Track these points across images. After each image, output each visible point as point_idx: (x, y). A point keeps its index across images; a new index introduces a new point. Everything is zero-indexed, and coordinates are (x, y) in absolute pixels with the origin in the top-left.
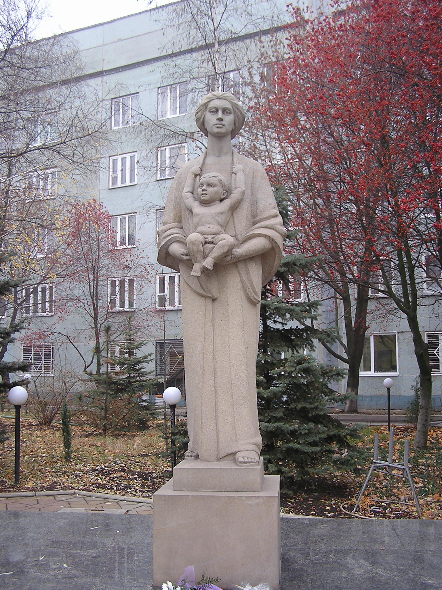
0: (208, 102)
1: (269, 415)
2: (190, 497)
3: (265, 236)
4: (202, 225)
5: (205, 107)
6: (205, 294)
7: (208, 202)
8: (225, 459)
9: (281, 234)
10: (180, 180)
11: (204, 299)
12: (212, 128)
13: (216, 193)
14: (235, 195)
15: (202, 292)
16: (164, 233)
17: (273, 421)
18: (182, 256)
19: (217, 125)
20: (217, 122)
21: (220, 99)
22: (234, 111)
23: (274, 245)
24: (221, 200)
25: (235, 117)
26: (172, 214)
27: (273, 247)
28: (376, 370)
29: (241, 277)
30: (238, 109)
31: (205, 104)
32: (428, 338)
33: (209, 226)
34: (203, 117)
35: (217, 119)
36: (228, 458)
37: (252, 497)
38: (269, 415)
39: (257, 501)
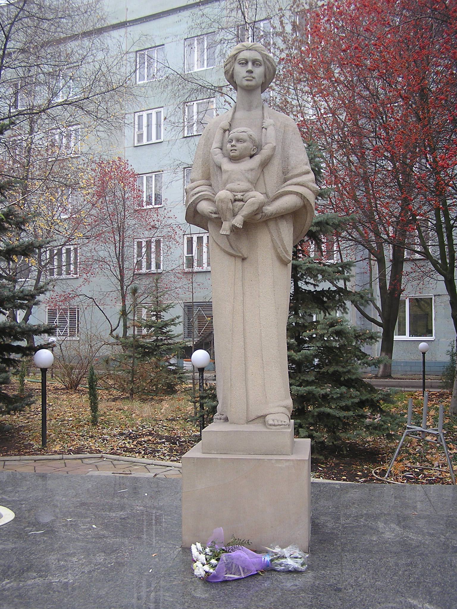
0: (237, 53)
1: (300, 378)
2: (219, 460)
3: (297, 193)
4: (231, 182)
7: (237, 158)
8: (254, 422)
9: (313, 192)
11: (233, 259)
13: (246, 148)
14: (266, 151)
15: (232, 251)
16: (192, 190)
18: (211, 214)
21: (250, 50)
22: (265, 63)
23: (306, 203)
24: (251, 156)
25: (265, 69)
26: (200, 171)
27: (305, 204)
29: (272, 236)
30: (268, 60)
31: (234, 55)
33: (238, 183)
36: (257, 421)
38: (300, 378)
39: (287, 464)
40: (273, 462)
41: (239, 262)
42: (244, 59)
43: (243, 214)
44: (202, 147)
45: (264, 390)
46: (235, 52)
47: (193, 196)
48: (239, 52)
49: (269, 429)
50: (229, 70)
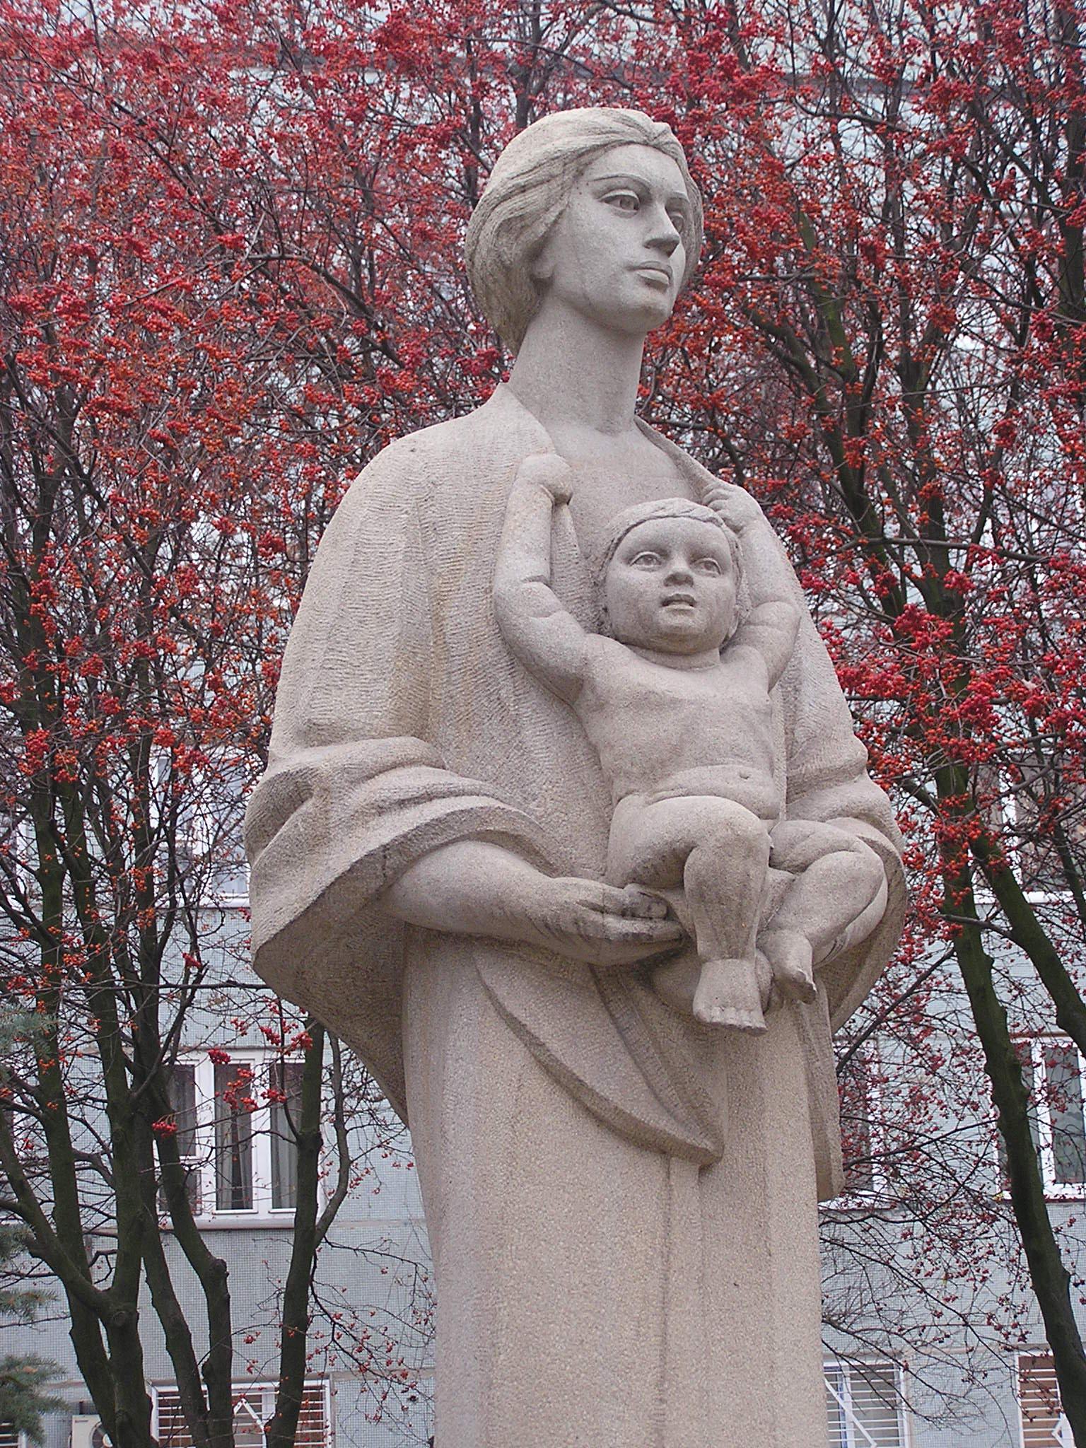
0: (594, 149)
10: (431, 515)
11: (650, 1166)
12: (615, 278)
16: (355, 782)
18: (596, 917)
20: (651, 256)
21: (657, 147)
26: (383, 689)
34: (551, 217)
35: (648, 245)
41: (683, 1175)
42: (637, 181)
43: (813, 930)
44: (398, 567)
46: (583, 142)
47: (381, 810)
48: (606, 147)
50: (536, 216)
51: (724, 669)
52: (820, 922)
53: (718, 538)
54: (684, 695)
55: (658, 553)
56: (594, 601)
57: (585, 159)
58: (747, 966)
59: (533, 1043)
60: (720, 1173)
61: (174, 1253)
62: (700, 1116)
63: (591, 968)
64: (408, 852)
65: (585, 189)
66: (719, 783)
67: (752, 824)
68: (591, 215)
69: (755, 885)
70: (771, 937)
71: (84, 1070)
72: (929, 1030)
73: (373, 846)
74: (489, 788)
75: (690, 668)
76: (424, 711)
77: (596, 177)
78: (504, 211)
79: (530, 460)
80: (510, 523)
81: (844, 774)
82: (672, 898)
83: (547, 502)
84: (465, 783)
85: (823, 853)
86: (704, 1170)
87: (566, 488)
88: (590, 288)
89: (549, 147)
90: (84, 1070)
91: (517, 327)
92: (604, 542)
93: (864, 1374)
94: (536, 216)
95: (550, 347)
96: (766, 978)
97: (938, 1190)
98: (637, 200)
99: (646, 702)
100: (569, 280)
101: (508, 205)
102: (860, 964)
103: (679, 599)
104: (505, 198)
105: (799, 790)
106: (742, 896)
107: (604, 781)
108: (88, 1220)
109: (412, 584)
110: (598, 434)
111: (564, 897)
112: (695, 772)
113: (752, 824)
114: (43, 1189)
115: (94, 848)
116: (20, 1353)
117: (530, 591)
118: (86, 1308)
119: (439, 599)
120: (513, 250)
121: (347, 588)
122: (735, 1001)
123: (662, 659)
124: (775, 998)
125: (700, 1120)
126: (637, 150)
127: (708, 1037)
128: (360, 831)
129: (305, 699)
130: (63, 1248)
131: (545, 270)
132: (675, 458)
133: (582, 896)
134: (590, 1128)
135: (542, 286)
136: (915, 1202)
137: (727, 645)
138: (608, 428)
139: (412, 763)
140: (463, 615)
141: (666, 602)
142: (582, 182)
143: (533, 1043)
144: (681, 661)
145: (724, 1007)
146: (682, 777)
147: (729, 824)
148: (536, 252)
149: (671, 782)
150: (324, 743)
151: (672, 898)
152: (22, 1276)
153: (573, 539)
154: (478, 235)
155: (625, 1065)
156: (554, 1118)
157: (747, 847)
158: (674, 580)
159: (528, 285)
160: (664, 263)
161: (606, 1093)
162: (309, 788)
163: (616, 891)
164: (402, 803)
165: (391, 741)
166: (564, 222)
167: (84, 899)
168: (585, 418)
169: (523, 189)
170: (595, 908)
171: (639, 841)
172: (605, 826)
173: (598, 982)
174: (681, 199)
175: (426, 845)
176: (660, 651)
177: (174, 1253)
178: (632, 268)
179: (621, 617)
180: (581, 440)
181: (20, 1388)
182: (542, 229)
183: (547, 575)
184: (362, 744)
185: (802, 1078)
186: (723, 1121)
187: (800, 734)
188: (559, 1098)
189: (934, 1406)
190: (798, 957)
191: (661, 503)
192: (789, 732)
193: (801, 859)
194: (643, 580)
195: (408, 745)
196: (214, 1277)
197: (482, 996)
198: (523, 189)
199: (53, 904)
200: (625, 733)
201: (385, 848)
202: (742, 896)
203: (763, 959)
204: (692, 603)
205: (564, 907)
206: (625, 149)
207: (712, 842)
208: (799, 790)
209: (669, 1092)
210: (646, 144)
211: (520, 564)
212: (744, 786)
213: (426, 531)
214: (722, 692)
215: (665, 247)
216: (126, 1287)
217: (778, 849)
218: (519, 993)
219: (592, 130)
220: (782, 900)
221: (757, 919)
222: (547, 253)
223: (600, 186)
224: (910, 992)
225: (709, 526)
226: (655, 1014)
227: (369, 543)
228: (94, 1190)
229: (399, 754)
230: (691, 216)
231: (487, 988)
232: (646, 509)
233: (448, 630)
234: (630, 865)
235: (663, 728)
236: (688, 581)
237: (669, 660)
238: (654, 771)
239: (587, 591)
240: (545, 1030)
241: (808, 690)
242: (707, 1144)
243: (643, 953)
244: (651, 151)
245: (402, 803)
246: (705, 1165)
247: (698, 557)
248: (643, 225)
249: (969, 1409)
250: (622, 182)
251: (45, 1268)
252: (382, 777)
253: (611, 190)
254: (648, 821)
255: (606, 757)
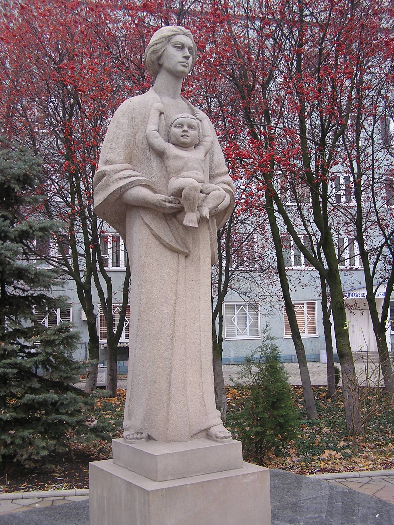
0: (172, 35)
1: (25, 386)
2: (189, 487)
4: (188, 170)
5: (167, 39)
6: (178, 247)
7: (187, 146)
8: (196, 436)
10: (134, 116)
11: (175, 255)
12: (176, 64)
16: (115, 173)
17: (29, 392)
18: (164, 203)
19: (182, 64)
20: (184, 60)
21: (186, 35)
26: (122, 153)
28: (309, 333)
31: (169, 36)
32: (70, 312)
34: (163, 50)
35: (183, 57)
36: (199, 435)
37: (247, 474)
38: (25, 386)
39: (252, 478)
40: (240, 477)
41: (182, 258)
42: (181, 43)
43: (210, 207)
44: (126, 127)
45: (204, 401)
46: (170, 34)
48: (175, 35)
49: (221, 442)
50: (159, 50)
51: (195, 151)
52: (211, 205)
53: (195, 122)
54: (185, 156)
55: (181, 125)
56: (168, 135)
57: (170, 37)
58: (195, 214)
59: (151, 229)
60: (190, 257)
61: (100, 276)
62: (185, 245)
63: (164, 214)
64: (125, 188)
65: (170, 44)
66: (191, 175)
67: (196, 183)
68: (171, 50)
69: (197, 197)
70: (201, 208)
71: (80, 236)
72: (266, 232)
73: (118, 187)
74: (144, 175)
75: (187, 150)
76: (131, 158)
77: (173, 40)
78: (152, 49)
79: (155, 104)
80: (150, 118)
81: (223, 174)
82: (180, 199)
83: (158, 114)
84: (138, 174)
85: (213, 190)
86: (186, 257)
87: (163, 111)
88: (170, 67)
89: (162, 35)
90: (80, 236)
91: (156, 74)
92: (170, 123)
93: (251, 305)
94: (159, 50)
95: (162, 79)
96: (199, 217)
97: (266, 266)
98: (182, 47)
99: (177, 157)
100: (166, 65)
101: (153, 47)
102: (225, 215)
103: (185, 135)
104: (153, 46)
105: (212, 178)
106: (194, 199)
107: (168, 174)
108: (81, 268)
109: (129, 131)
110: (172, 99)
111: (157, 198)
112: (186, 173)
113: (196, 183)
114: (71, 261)
115: (83, 187)
116: (62, 295)
117: (153, 133)
118: (80, 287)
119: (135, 134)
120: (154, 58)
121: (115, 131)
122: (192, 221)
123: (181, 148)
124: (201, 221)
125: (186, 246)
126: (182, 36)
127: (188, 229)
128: (116, 183)
129: (106, 155)
130: (75, 274)
131: (161, 62)
132: (188, 104)
133: (161, 198)
134: (163, 248)
135: (161, 66)
136: (262, 270)
137: (196, 146)
138: (174, 98)
139: (128, 169)
140: (140, 138)
141: (182, 136)
142: (169, 43)
143: (151, 229)
144: (185, 149)
145: (189, 222)
146: (184, 174)
147: (191, 184)
148: (159, 58)
149: (181, 175)
150: (109, 165)
151: (180, 199)
152: (68, 279)
153: (164, 122)
154: (148, 55)
155: (170, 234)
156: (155, 245)
157: (195, 189)
158: (184, 131)
159: (158, 65)
160: (187, 61)
161: (166, 240)
162: (105, 174)
163: (168, 198)
164: (125, 178)
165: (123, 164)
166: (165, 52)
167: (80, 199)
168: (169, 95)
169: (156, 44)
170: (163, 201)
171: (173, 187)
172: (168, 183)
173: (165, 217)
174: (191, 47)
175: (129, 187)
176: (181, 147)
177: (100, 276)
178: (180, 62)
179: (173, 139)
180: (167, 100)
181: (61, 301)
182: (160, 53)
183: (157, 129)
184: (117, 165)
185: (209, 238)
186: (191, 247)
187: (213, 165)
188: (156, 241)
189: (265, 312)
190: (206, 212)
191: (182, 114)
192: (211, 165)
193: (208, 192)
194: (177, 131)
195: (127, 165)
196: (109, 281)
197: (141, 219)
198: (156, 44)
199: (73, 199)
200: (172, 164)
201: (121, 187)
202: (194, 199)
203: (198, 212)
204: (188, 136)
205: (157, 200)
206: (179, 35)
207: (188, 188)
208: (212, 178)
209: (180, 240)
210: (184, 34)
211: (152, 127)
212: (197, 176)
213: (132, 119)
214: (194, 156)
215: (187, 58)
216: (88, 282)
217: (204, 190)
218: (148, 218)
219: (172, 31)
220: (204, 200)
221: (197, 204)
222: (162, 59)
223: (173, 44)
224: (262, 223)
225: (193, 120)
226: (177, 224)
227: (120, 122)
228: (82, 262)
229: (124, 167)
230: (194, 51)
231: (142, 217)
232: (179, 116)
233: (137, 141)
234: (171, 192)
235: (179, 163)
236: (187, 131)
237: (183, 148)
238: (178, 172)
239: (166, 133)
240: (153, 227)
241: (216, 156)
242: (187, 251)
243: (174, 211)
244: (185, 36)
245: (125, 178)
246: (187, 256)
247: (190, 126)
248: (183, 53)
249: (273, 313)
250: (178, 43)
251: (72, 278)
252: (125, 171)
253: (175, 44)
254: (176, 182)
255: (168, 169)
